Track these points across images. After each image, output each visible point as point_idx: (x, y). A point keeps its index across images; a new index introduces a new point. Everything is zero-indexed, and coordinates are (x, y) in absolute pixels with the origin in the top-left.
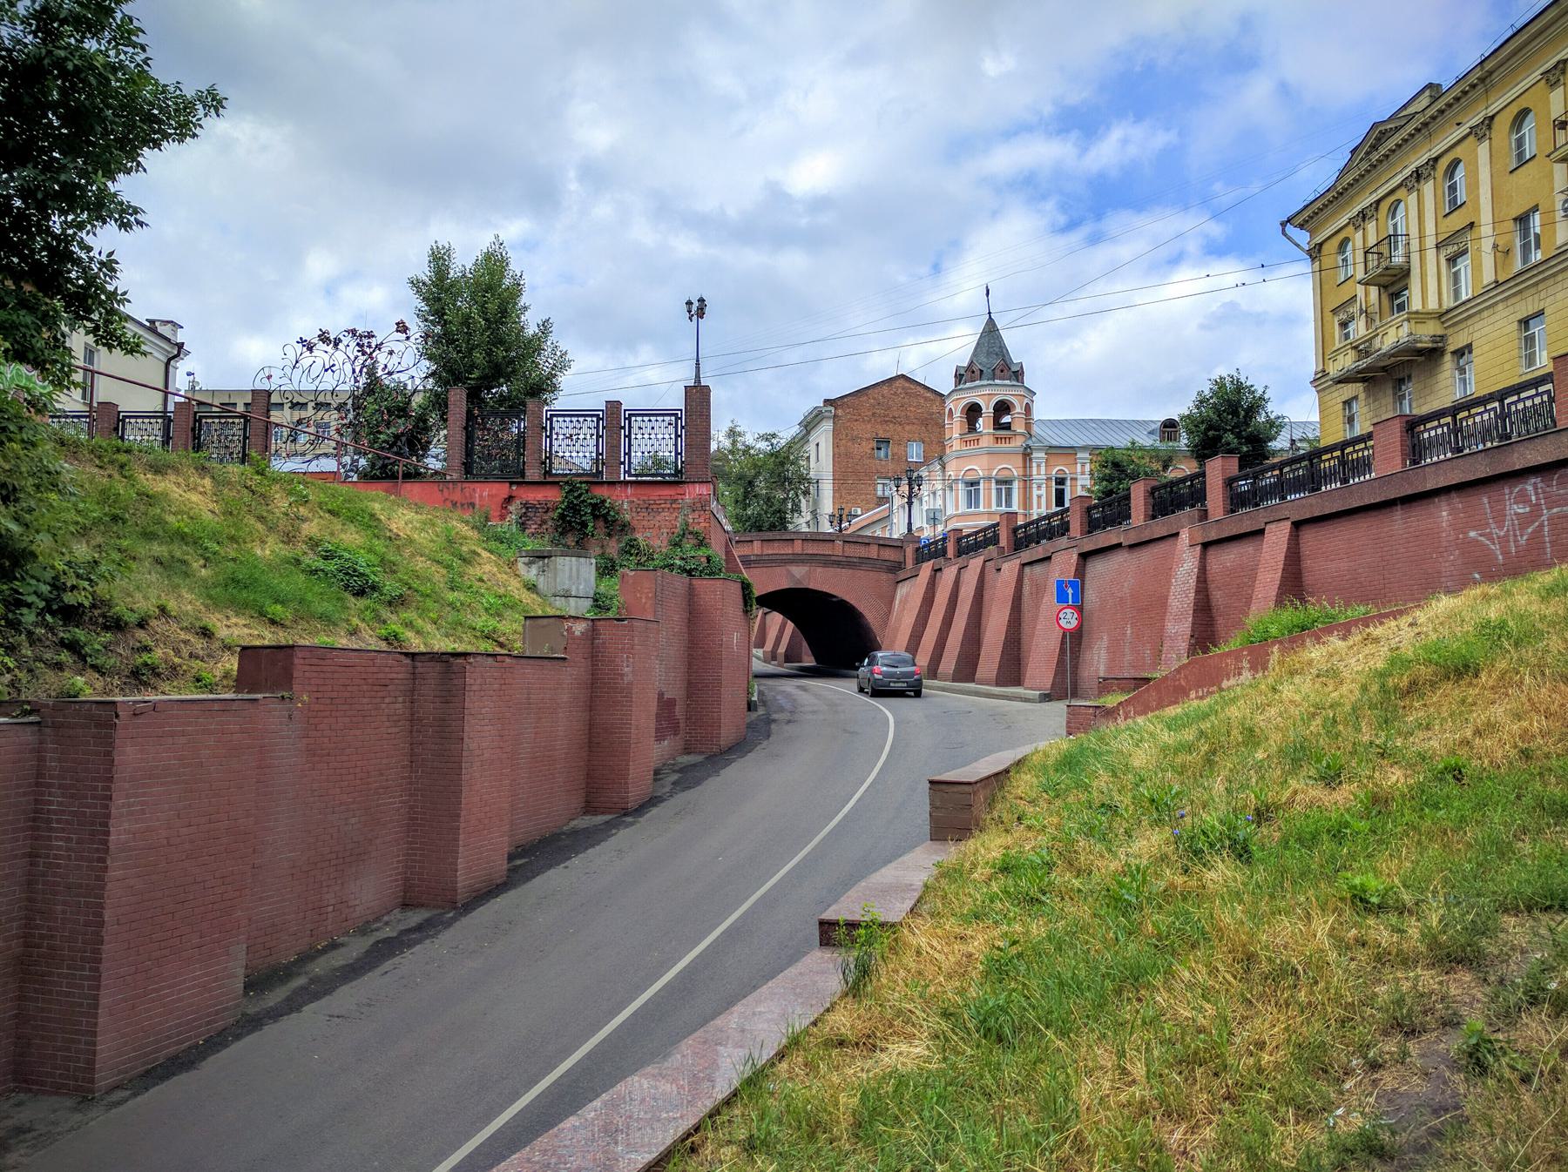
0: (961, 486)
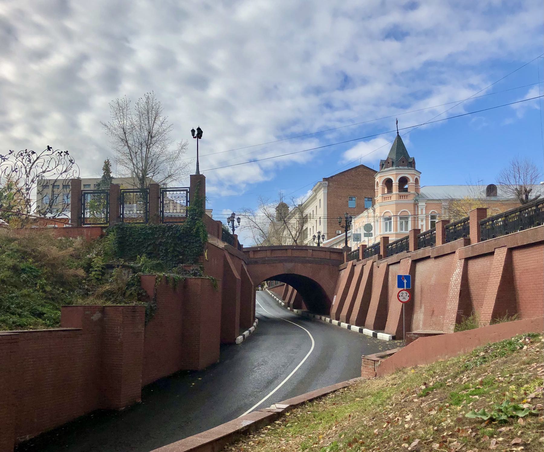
0: (382, 220)
